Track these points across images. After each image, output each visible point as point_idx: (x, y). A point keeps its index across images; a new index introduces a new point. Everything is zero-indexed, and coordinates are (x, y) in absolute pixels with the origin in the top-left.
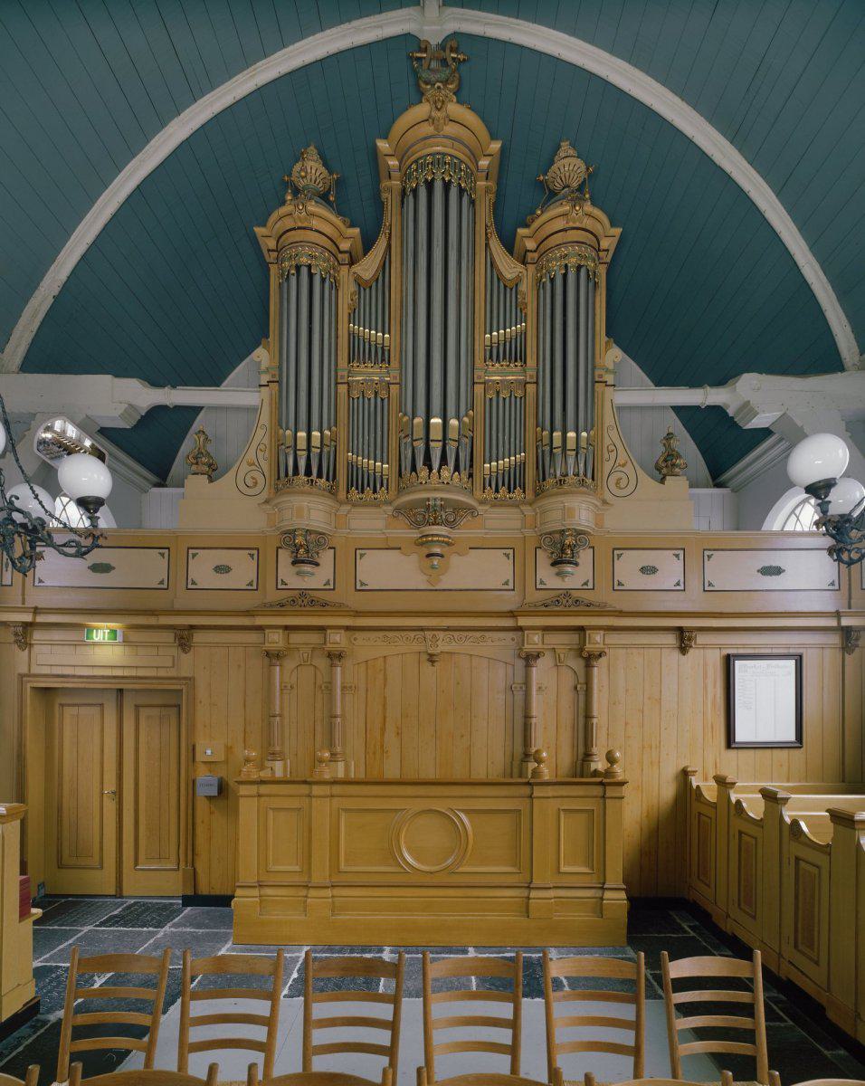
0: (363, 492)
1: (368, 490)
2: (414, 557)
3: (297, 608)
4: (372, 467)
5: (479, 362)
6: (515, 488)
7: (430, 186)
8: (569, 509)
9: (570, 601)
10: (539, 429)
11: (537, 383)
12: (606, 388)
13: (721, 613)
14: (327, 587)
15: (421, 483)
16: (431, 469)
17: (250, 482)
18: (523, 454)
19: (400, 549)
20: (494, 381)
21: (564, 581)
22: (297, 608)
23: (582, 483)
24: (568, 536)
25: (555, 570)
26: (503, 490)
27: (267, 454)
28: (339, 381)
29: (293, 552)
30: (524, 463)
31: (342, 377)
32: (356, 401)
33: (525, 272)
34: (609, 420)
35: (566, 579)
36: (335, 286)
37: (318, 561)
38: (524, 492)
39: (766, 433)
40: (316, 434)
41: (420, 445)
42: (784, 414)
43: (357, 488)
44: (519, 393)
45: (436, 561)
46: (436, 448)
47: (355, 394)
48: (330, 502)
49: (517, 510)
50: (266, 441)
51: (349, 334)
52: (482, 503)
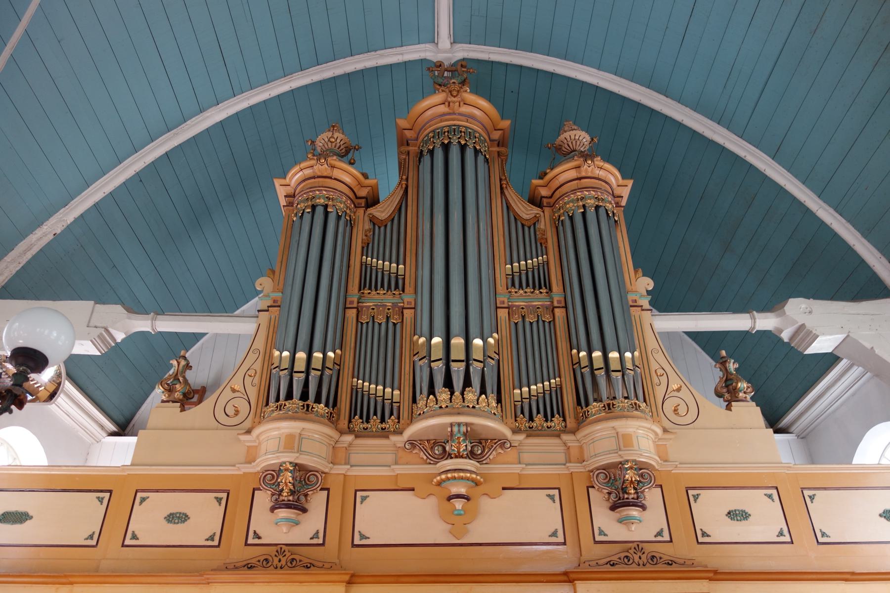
0: (368, 421)
1: (375, 420)
2: (432, 501)
3: (634, 567)
4: (380, 393)
5: (501, 288)
6: (553, 416)
7: (446, 148)
8: (623, 435)
9: (644, 557)
10: (575, 351)
11: (566, 307)
12: (642, 312)
13: (853, 573)
14: (315, 541)
15: (441, 407)
16: (452, 393)
17: (230, 411)
18: (558, 379)
19: (413, 490)
20: (518, 306)
21: (629, 530)
22: (634, 567)
23: (637, 407)
24: (627, 469)
25: (614, 515)
26: (539, 419)
27: (256, 380)
28: (348, 306)
29: (273, 495)
30: (561, 388)
31: (352, 302)
32: (365, 326)
33: (542, 214)
34: (651, 343)
35: (633, 527)
36: (351, 224)
37: (306, 506)
38: (564, 420)
39: (829, 360)
40: (318, 355)
41: (439, 366)
42: (848, 336)
43: (361, 417)
44: (548, 318)
45: (459, 504)
46: (458, 369)
47: (364, 319)
48: (328, 431)
49: (556, 441)
50: (258, 366)
51: (362, 265)
52: (516, 431)
